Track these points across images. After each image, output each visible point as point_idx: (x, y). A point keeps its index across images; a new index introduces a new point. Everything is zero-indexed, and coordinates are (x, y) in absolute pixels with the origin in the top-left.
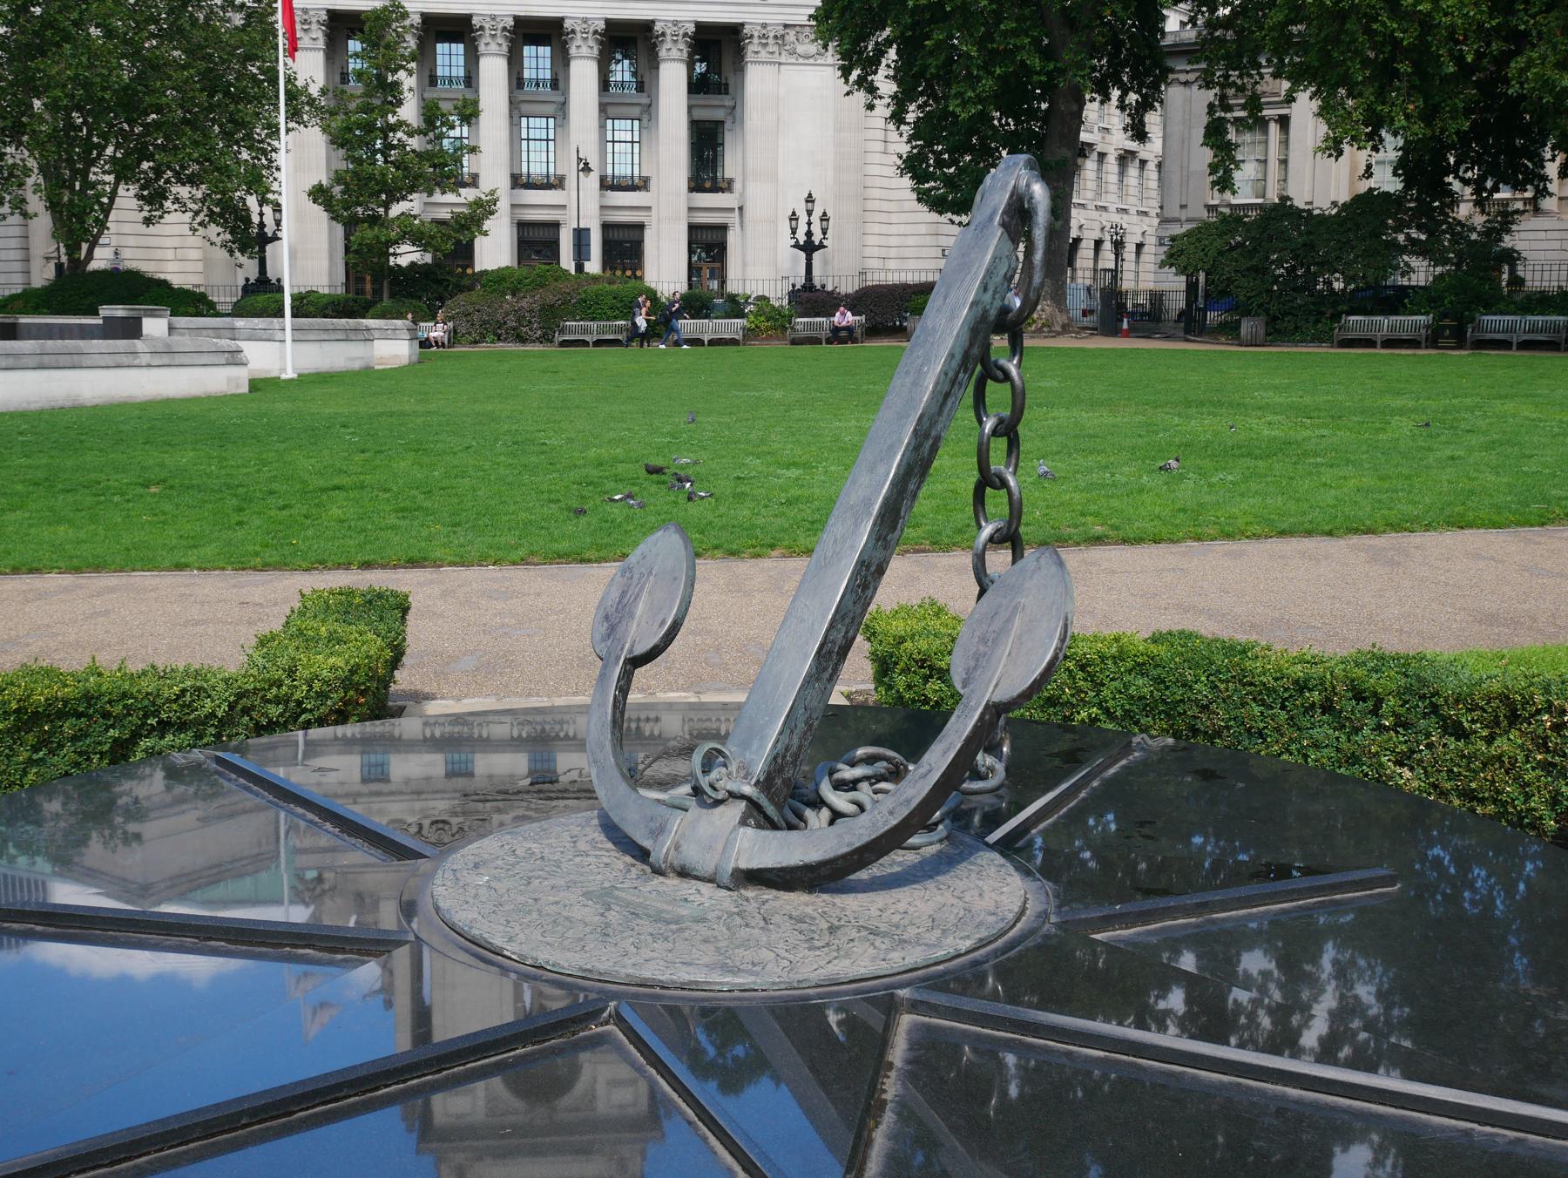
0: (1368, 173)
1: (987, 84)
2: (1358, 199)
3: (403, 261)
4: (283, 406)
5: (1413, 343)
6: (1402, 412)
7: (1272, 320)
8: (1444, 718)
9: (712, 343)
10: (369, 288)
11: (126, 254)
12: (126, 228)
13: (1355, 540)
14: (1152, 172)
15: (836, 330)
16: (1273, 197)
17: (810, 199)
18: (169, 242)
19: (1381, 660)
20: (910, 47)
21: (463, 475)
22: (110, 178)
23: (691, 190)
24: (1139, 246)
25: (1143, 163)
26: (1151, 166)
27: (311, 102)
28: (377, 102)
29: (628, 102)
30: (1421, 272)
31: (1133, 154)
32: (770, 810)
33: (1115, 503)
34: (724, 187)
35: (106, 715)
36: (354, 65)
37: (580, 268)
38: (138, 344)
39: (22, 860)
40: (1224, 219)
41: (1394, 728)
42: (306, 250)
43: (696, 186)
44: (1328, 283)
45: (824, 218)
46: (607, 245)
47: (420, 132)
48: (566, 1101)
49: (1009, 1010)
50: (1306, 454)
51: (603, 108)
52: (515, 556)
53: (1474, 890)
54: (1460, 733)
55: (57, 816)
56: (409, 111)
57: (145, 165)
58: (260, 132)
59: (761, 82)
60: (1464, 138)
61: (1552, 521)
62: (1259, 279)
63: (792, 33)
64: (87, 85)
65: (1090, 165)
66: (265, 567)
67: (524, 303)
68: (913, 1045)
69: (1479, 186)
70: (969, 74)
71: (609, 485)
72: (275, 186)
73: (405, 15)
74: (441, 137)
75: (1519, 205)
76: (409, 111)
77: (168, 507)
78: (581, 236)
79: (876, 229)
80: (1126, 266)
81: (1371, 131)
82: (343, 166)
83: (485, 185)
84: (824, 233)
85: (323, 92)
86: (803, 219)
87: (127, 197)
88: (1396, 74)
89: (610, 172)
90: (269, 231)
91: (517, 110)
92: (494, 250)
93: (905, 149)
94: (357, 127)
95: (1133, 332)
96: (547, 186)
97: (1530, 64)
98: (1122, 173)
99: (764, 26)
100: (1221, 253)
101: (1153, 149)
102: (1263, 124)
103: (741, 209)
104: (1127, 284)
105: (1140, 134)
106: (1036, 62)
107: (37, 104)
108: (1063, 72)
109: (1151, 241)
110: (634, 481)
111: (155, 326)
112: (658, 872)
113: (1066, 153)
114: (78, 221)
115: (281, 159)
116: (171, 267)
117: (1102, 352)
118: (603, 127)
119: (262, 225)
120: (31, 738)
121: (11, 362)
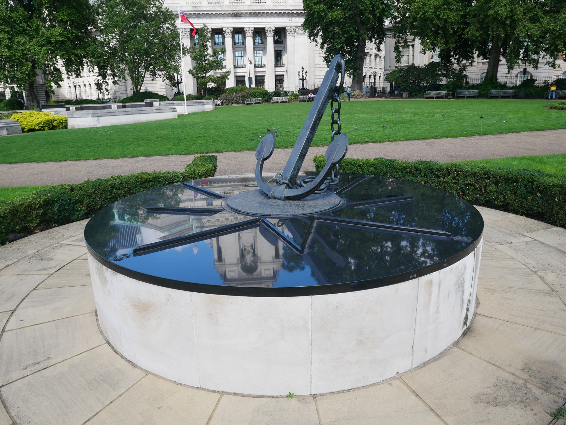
0: (432, 57)
1: (343, 39)
2: (430, 64)
3: (210, 86)
4: (186, 120)
5: (442, 97)
6: (438, 113)
7: (410, 93)
8: (435, 174)
9: (281, 102)
10: (203, 92)
11: (148, 88)
12: (148, 82)
13: (424, 141)
14: (382, 58)
15: (309, 98)
16: (410, 64)
17: (303, 68)
18: (157, 85)
19: (422, 162)
20: (325, 31)
21: (227, 133)
22: (144, 70)
24: (380, 77)
25: (380, 57)
26: (382, 57)
27: (188, 50)
28: (202, 49)
29: (260, 47)
30: (444, 81)
31: (378, 54)
32: (291, 186)
33: (371, 134)
34: (283, 66)
35: (158, 181)
36: (197, 41)
37: (250, 86)
38: (153, 108)
39: (135, 223)
40: (399, 69)
41: (424, 176)
42: (188, 85)
43: (276, 66)
44: (423, 84)
45: (306, 72)
46: (256, 80)
47: (212, 56)
48: (255, 274)
49: (336, 218)
50: (415, 123)
51: (254, 48)
52: (239, 149)
53: (455, 221)
54: (437, 176)
55: (142, 214)
56: (210, 51)
57: (151, 67)
58: (176, 58)
59: (290, 40)
60: (454, 49)
61: (468, 136)
62: (407, 83)
64: (137, 49)
65: (368, 57)
66: (185, 154)
67: (238, 95)
68: (317, 224)
69: (458, 60)
70: (339, 37)
71: (259, 134)
72: (180, 70)
73: (208, 29)
74: (217, 57)
75: (468, 64)
76: (210, 51)
77: (163, 142)
78: (250, 79)
79: (318, 74)
80: (376, 81)
81: (433, 47)
82: (195, 65)
83: (228, 68)
85: (190, 48)
86: (301, 73)
87: (148, 74)
88: (439, 33)
91: (234, 50)
92: (230, 83)
93: (324, 55)
94: (198, 56)
95: (378, 97)
97: (470, 30)
98: (375, 59)
100: (398, 77)
101: (382, 53)
102: (408, 46)
104: (377, 85)
105: (379, 50)
106: (354, 33)
107: (126, 54)
108: (361, 35)
109: (382, 75)
110: (264, 133)
111: (156, 104)
112: (270, 198)
113: (362, 55)
114: (137, 81)
115: (181, 64)
116: (158, 90)
117: (371, 101)
118: (254, 53)
119: (178, 80)
120: (143, 186)
121: (126, 113)
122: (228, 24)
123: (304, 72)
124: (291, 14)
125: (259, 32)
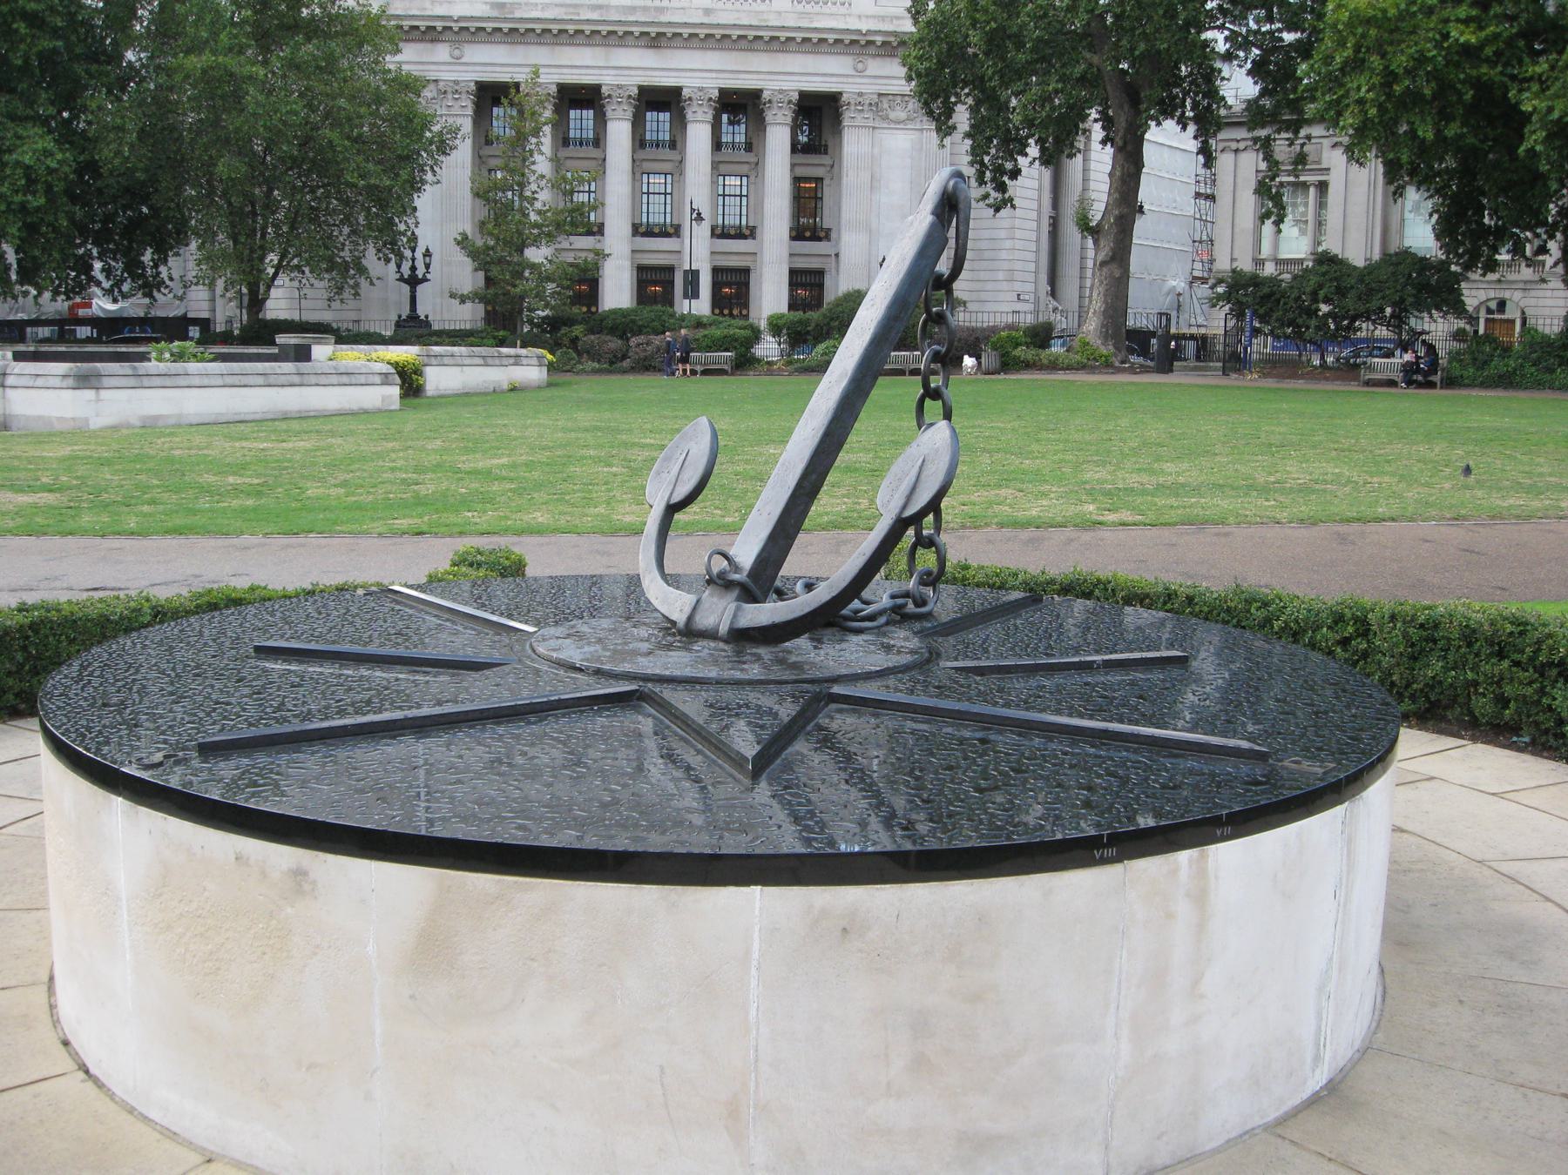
5: (721, 372)
23: (793, 238)
45: (427, 254)
46: (716, 286)
51: (715, 165)
59: (855, 143)
63: (885, 100)
84: (427, 266)
89: (720, 222)
90: (420, 272)
96: (664, 234)
99: (860, 94)
103: (837, 255)
111: (322, 351)
118: (714, 183)
122: (622, 70)
123: (419, 254)
124: (857, 45)
125: (739, 106)
